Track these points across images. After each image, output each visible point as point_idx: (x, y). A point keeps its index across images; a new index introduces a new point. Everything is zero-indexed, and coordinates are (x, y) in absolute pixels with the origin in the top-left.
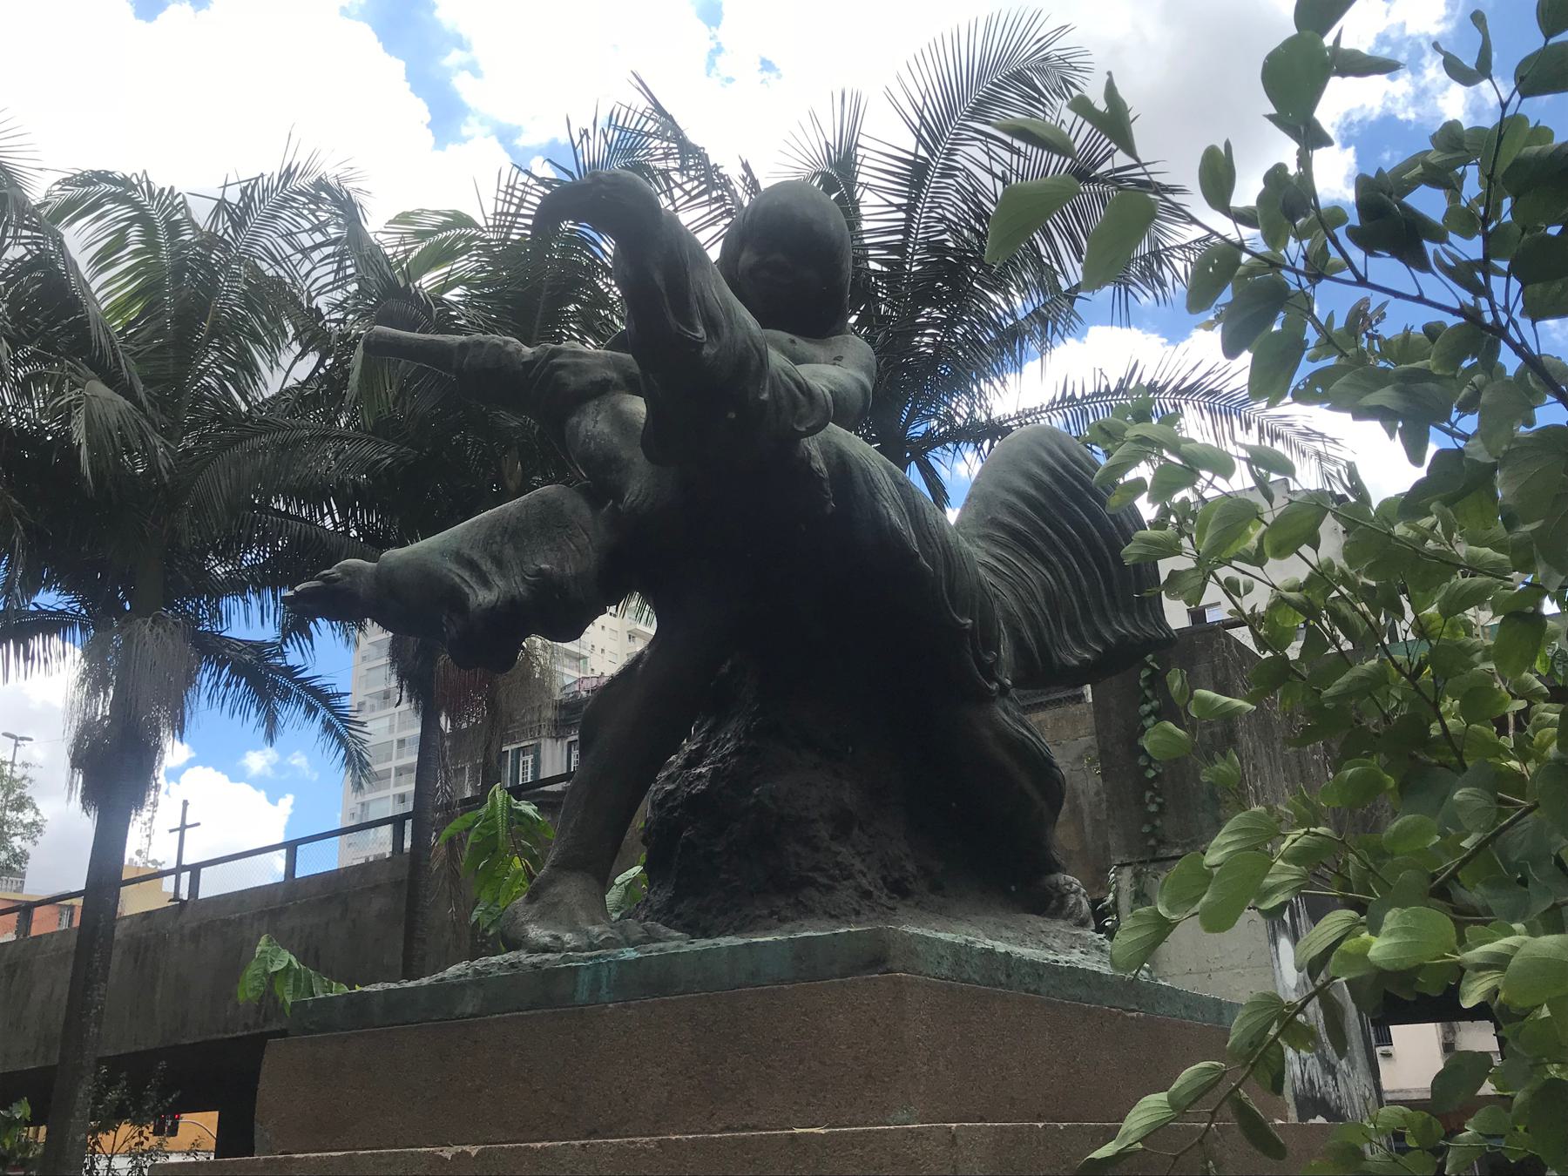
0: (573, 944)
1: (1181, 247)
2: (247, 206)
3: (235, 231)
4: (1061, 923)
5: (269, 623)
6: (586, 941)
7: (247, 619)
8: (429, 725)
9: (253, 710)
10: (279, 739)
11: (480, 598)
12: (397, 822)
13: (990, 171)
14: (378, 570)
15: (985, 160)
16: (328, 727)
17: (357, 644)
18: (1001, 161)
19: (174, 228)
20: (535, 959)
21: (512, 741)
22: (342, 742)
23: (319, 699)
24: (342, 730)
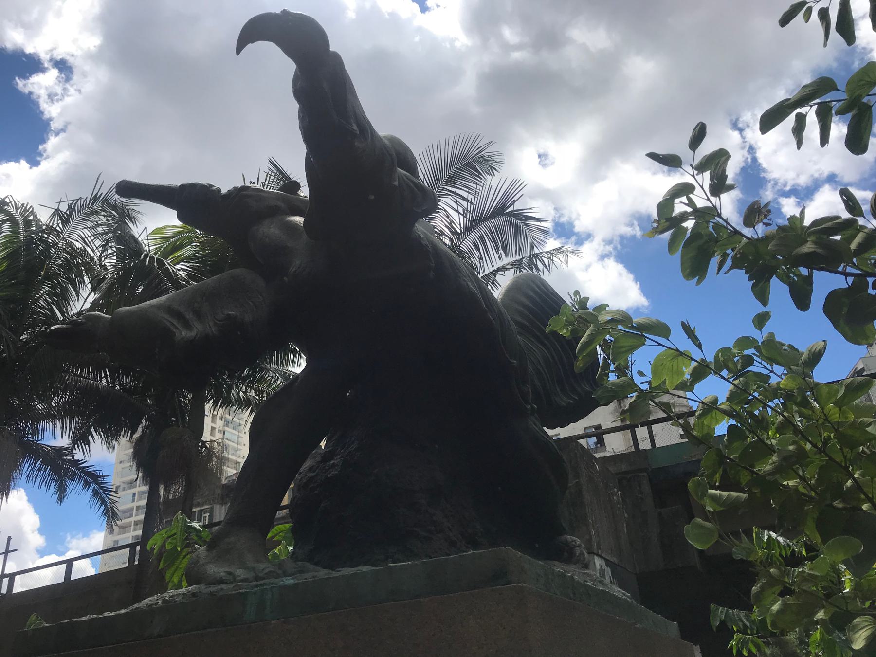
0: (243, 576)
1: (547, 253)
2: (71, 213)
3: (63, 226)
4: (574, 566)
5: (66, 437)
6: (252, 575)
7: (53, 434)
8: (152, 494)
9: (53, 484)
10: (66, 502)
11: (184, 334)
12: (132, 546)
13: (457, 211)
14: (111, 321)
15: (455, 206)
16: (96, 494)
17: (114, 448)
18: (462, 206)
19: (28, 224)
20: (212, 589)
21: (198, 505)
22: (103, 502)
23: (93, 479)
24: (103, 495)
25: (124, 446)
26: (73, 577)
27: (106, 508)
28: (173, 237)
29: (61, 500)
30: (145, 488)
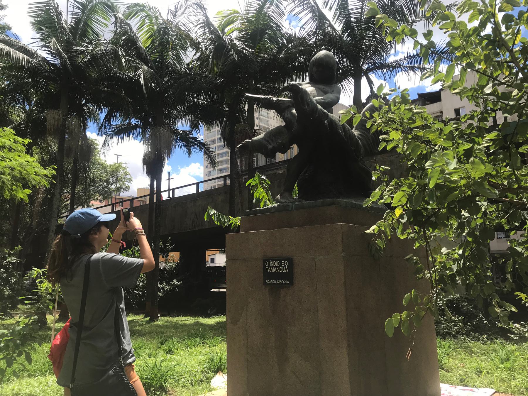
2: (176, 11)
10: (192, 156)
16: (205, 153)
22: (208, 155)
25: (216, 130)
26: (200, 191)
27: (211, 160)
28: (227, 16)
29: (189, 156)
30: (226, 150)
